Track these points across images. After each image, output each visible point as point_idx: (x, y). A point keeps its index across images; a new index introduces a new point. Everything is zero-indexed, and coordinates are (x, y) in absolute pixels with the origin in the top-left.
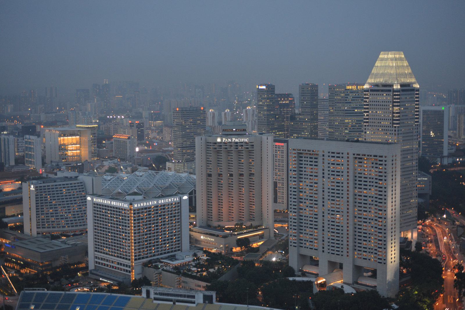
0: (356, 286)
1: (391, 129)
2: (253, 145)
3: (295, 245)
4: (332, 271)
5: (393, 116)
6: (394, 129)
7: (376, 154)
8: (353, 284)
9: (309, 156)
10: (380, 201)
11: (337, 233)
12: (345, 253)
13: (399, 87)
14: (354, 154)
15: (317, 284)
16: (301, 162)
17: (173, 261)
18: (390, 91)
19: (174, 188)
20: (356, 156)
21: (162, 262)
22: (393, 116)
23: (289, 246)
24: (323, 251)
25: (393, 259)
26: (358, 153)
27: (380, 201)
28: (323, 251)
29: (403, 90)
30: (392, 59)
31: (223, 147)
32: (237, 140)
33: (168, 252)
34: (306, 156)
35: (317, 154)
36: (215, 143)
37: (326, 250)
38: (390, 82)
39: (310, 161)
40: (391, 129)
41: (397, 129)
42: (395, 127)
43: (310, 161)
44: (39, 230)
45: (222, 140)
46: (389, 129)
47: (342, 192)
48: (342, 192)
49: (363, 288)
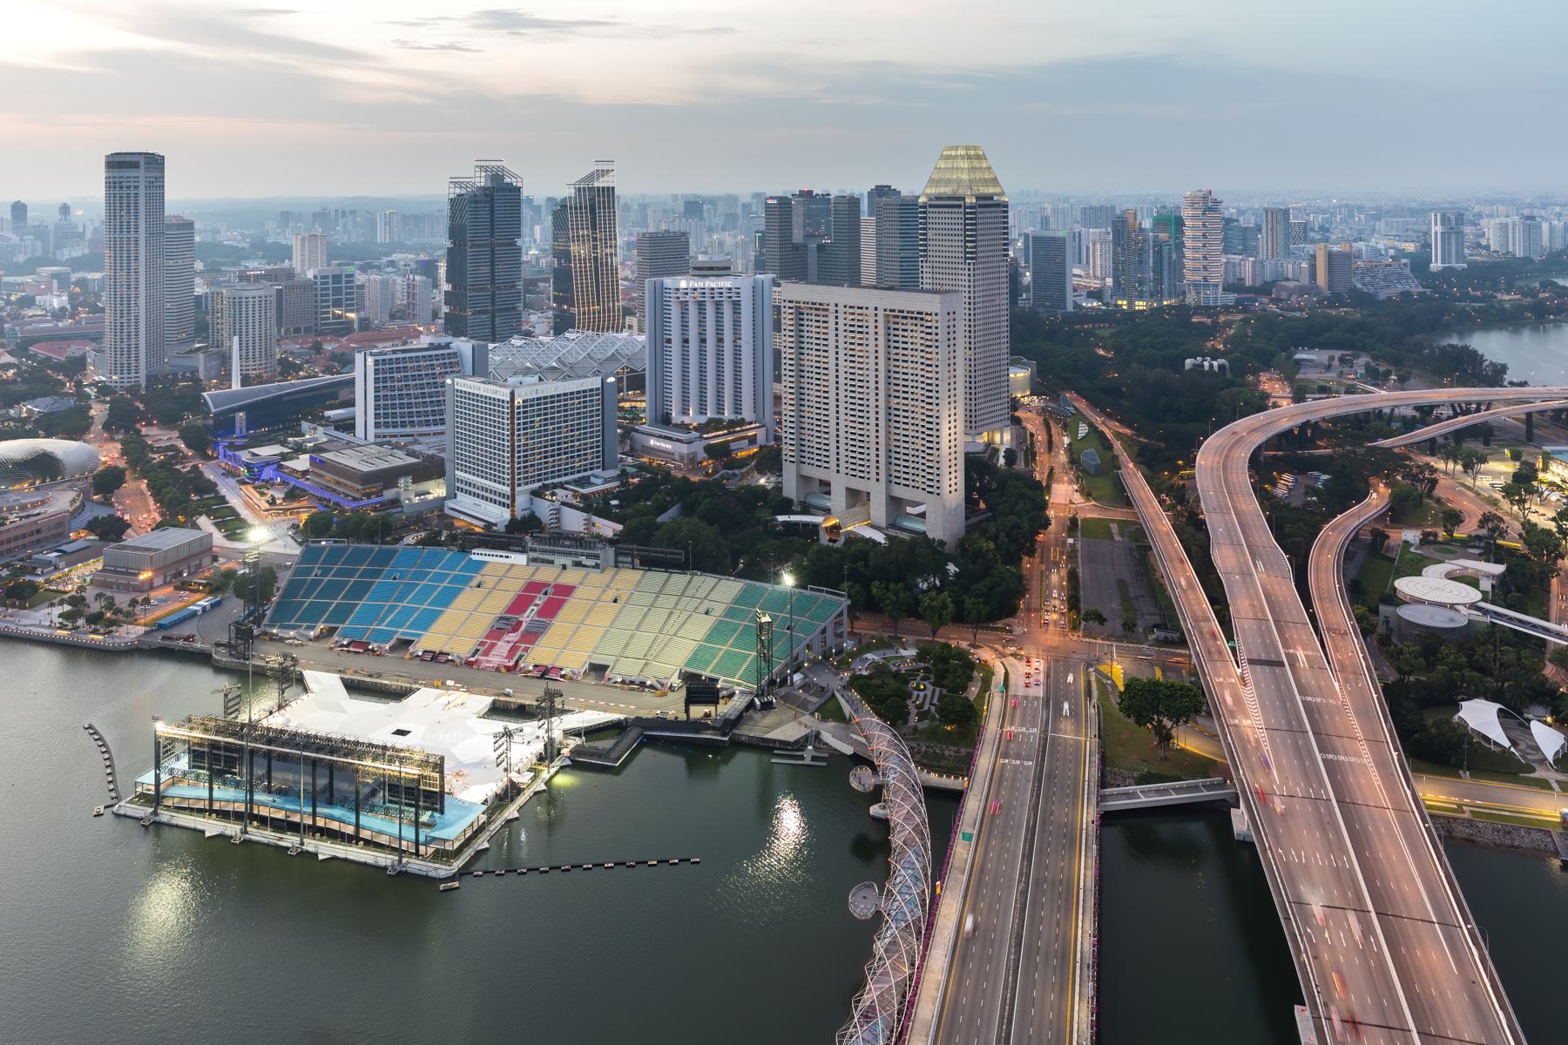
0: (892, 532)
1: (963, 266)
2: (739, 293)
3: (793, 459)
4: (854, 506)
5: (966, 247)
6: (967, 267)
7: (921, 310)
8: (887, 528)
9: (814, 312)
10: (930, 400)
11: (904, 398)
12: (873, 476)
13: (974, 200)
14: (885, 310)
15: (826, 528)
16: (802, 322)
17: (583, 488)
18: (959, 206)
19: (619, 360)
20: (888, 313)
21: (566, 489)
22: (966, 253)
23: (784, 462)
24: (838, 471)
25: (954, 487)
26: (893, 308)
27: (930, 400)
28: (838, 471)
29: (980, 206)
30: (963, 157)
31: (724, 295)
32: (713, 285)
33: (579, 472)
34: (810, 312)
35: (827, 310)
36: (678, 290)
37: (842, 469)
38: (961, 192)
39: (816, 321)
40: (963, 266)
41: (972, 267)
42: (969, 264)
43: (816, 321)
44: (379, 431)
45: (688, 284)
46: (960, 266)
47: (867, 373)
48: (867, 373)
49: (905, 536)
